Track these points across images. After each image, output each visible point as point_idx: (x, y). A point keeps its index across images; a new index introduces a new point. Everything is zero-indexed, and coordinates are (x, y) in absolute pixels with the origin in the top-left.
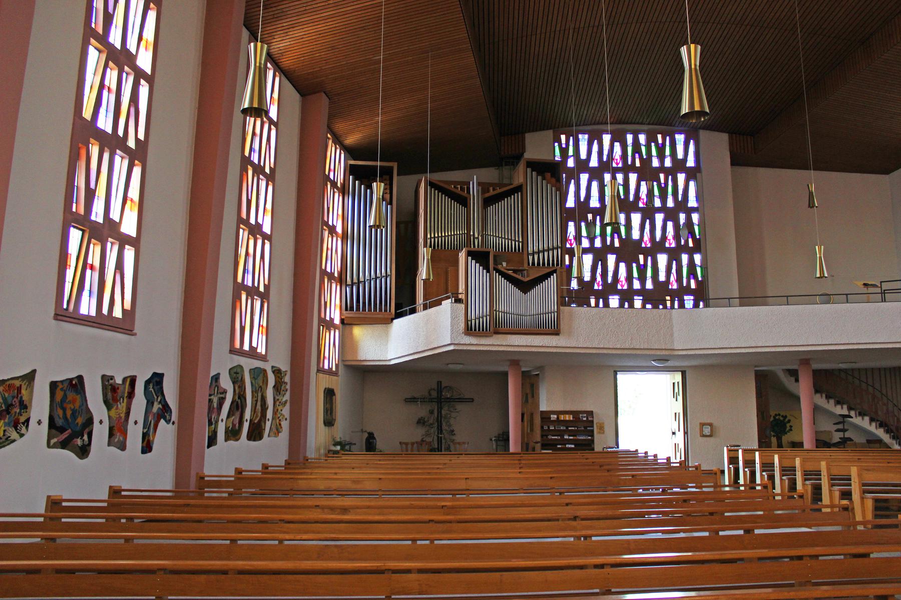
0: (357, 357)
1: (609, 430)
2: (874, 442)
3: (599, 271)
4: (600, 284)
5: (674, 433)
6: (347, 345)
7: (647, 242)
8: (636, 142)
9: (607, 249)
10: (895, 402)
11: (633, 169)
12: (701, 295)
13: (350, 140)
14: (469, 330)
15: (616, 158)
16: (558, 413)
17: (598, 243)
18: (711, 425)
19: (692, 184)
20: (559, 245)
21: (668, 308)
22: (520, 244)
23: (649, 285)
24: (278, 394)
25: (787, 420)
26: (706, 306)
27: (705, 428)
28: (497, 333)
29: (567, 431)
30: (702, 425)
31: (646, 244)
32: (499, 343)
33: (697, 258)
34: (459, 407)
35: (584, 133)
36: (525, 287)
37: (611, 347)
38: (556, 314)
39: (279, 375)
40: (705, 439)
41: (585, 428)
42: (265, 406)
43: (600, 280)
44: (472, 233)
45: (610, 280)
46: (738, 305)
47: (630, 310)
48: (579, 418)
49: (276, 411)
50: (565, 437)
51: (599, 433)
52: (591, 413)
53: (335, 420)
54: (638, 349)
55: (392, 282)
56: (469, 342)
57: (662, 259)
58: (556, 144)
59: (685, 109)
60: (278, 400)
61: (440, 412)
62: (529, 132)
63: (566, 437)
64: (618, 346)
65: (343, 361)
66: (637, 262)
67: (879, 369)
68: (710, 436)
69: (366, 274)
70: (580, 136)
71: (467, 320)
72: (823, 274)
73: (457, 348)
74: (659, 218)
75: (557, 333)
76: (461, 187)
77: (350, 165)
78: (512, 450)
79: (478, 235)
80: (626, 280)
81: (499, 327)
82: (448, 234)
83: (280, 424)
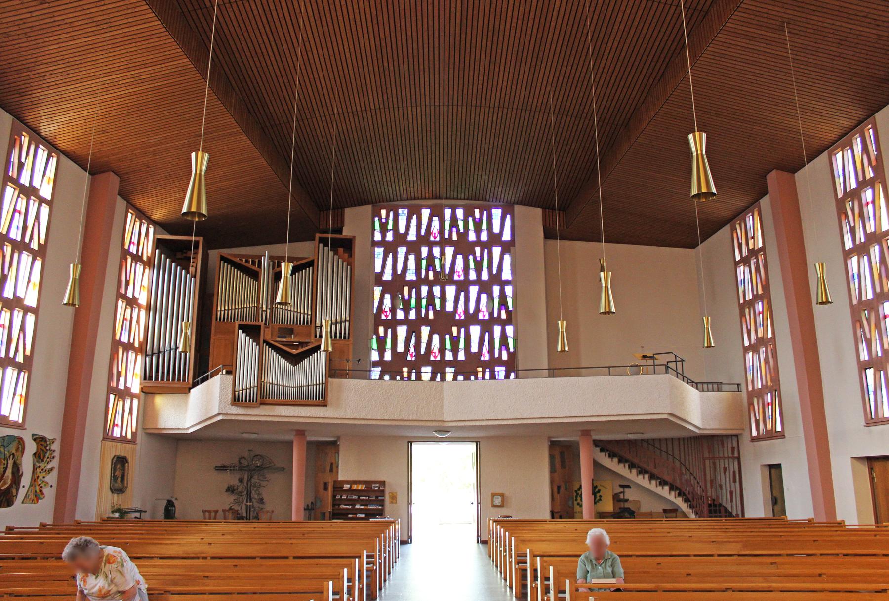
0: (157, 426)
1: (402, 499)
2: (672, 512)
3: (413, 342)
4: (414, 355)
5: (472, 503)
6: (147, 413)
7: (460, 314)
8: (454, 218)
9: (422, 321)
10: (692, 471)
11: (450, 242)
12: (511, 366)
13: (158, 215)
14: (236, 400)
15: (434, 232)
16: (352, 482)
17: (413, 315)
18: (502, 496)
19: (507, 257)
20: (348, 319)
21: (405, 379)
22: (309, 317)
23: (461, 356)
24: (40, 461)
25: (597, 490)
26: (517, 377)
27: (496, 499)
28: (262, 403)
29: (358, 501)
30: (493, 495)
31: (460, 316)
32: (266, 414)
33: (510, 330)
34: (269, 475)
35: (403, 207)
36: (295, 360)
37: (379, 418)
38: (324, 385)
39: (43, 443)
40: (497, 509)
41: (377, 497)
42: (19, 472)
43: (414, 351)
44: (260, 307)
45: (423, 351)
46: (547, 376)
47: (418, 382)
48: (371, 488)
49: (36, 478)
50: (356, 507)
51: (392, 503)
52: (383, 483)
53: (127, 487)
54: (406, 420)
55: (191, 355)
56: (236, 413)
57: (475, 331)
58: (377, 219)
59: (694, 191)
60: (39, 467)
61: (249, 480)
62: (348, 207)
63: (357, 506)
64: (386, 418)
65: (144, 429)
66: (451, 333)
67: (666, 439)
68: (501, 506)
69: (166, 344)
70: (400, 211)
71: (234, 391)
72: (564, 349)
73: (225, 418)
74: (474, 290)
75: (325, 405)
76: (252, 261)
77: (157, 239)
78: (294, 519)
79: (267, 308)
80: (439, 352)
81: (266, 398)
82: (232, 307)
83: (41, 491)
